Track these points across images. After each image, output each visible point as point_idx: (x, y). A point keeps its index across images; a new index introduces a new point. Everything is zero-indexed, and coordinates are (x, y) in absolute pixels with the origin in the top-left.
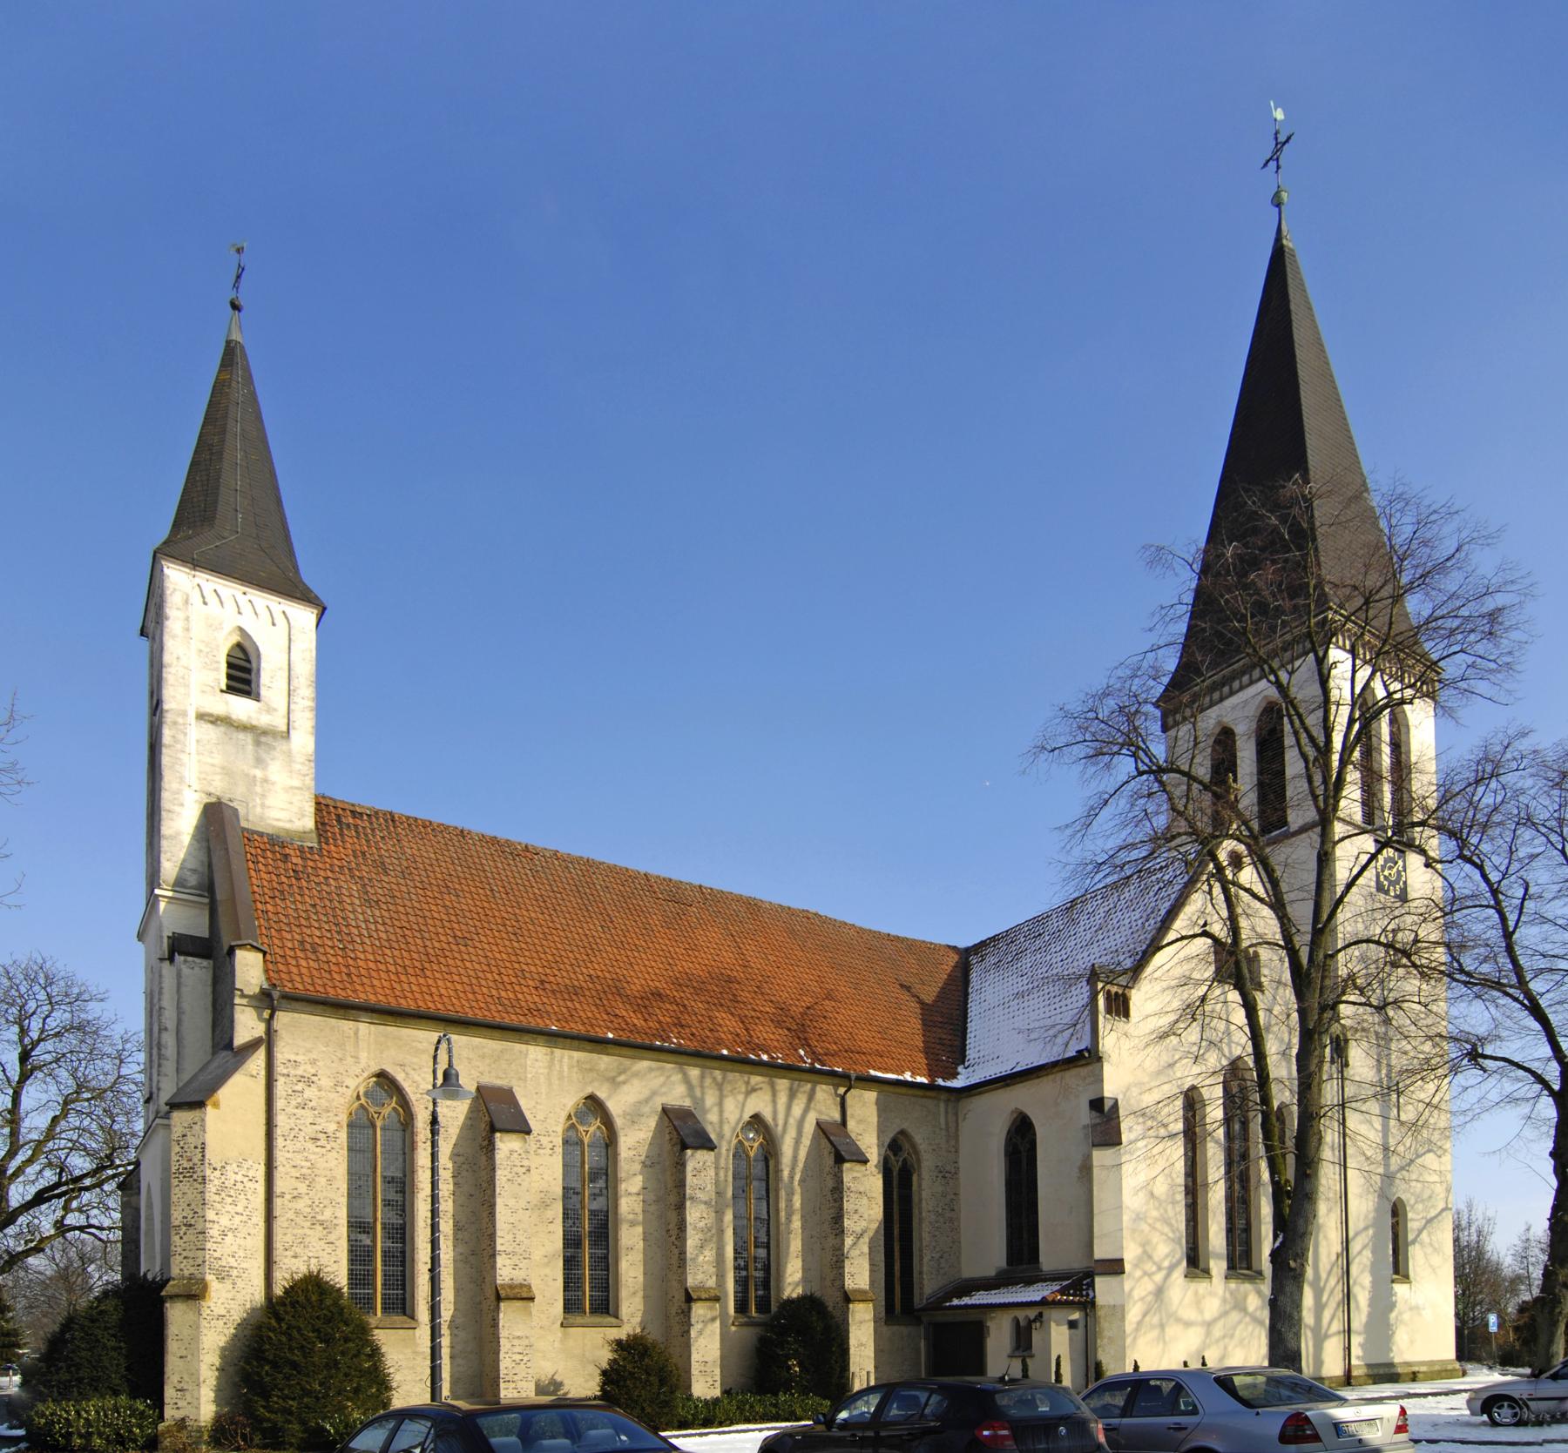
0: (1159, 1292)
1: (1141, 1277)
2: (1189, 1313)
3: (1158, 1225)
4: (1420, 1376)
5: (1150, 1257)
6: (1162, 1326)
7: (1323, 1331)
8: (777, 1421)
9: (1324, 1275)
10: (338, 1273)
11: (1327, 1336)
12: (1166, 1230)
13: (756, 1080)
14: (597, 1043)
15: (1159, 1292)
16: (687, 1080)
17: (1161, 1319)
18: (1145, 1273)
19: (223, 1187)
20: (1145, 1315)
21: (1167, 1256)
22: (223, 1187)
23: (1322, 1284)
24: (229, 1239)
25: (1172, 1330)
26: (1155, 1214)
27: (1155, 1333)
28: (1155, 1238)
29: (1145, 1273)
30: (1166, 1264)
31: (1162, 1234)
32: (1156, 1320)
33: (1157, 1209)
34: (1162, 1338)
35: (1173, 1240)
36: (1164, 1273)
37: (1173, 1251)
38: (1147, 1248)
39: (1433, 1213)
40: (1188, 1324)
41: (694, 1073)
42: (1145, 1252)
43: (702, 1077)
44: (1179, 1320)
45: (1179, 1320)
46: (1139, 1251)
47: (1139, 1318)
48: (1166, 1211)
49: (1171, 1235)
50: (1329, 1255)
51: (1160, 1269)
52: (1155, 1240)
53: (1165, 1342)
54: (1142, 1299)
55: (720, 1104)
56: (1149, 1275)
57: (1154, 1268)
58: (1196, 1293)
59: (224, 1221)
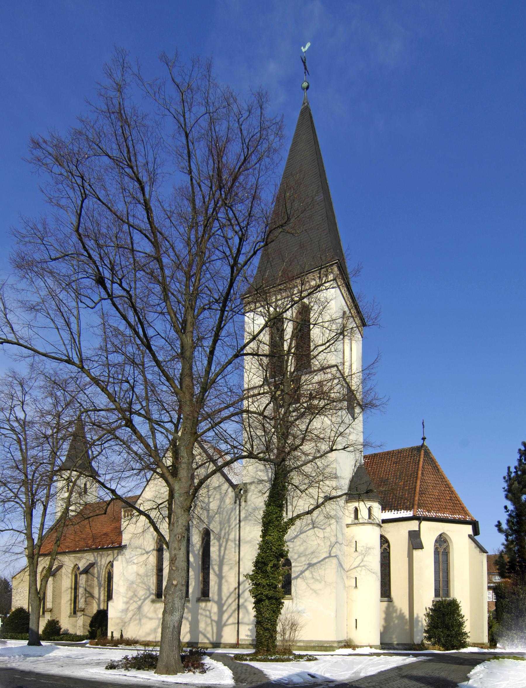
0: (140, 608)
1: (132, 603)
2: (151, 615)
3: (140, 585)
4: (222, 645)
5: (136, 596)
6: (140, 619)
7: (223, 623)
8: (415, 650)
9: (224, 598)
10: (26, 607)
11: (225, 625)
12: (143, 586)
13: (109, 552)
14: (75, 552)
15: (140, 608)
16: (94, 556)
17: (140, 617)
18: (134, 601)
19: (17, 592)
20: (133, 616)
21: (143, 595)
22: (17, 592)
23: (223, 602)
24: (18, 601)
25: (144, 621)
26: (139, 581)
27: (137, 622)
28: (139, 589)
29: (134, 601)
30: (143, 598)
31: (142, 587)
32: (138, 617)
33: (140, 579)
34: (140, 624)
35: (146, 589)
36: (141, 601)
37: (146, 593)
38: (136, 593)
39: (315, 561)
40: (151, 619)
41: (96, 554)
42: (134, 594)
43: (97, 555)
44: (147, 617)
45: (147, 617)
46: (132, 594)
47: (131, 616)
48: (144, 579)
49: (145, 587)
50: (229, 589)
51: (140, 600)
52: (138, 590)
53: (141, 625)
54: (133, 610)
55: (101, 561)
56: (136, 602)
57: (138, 600)
58: (155, 608)
59: (17, 598)
